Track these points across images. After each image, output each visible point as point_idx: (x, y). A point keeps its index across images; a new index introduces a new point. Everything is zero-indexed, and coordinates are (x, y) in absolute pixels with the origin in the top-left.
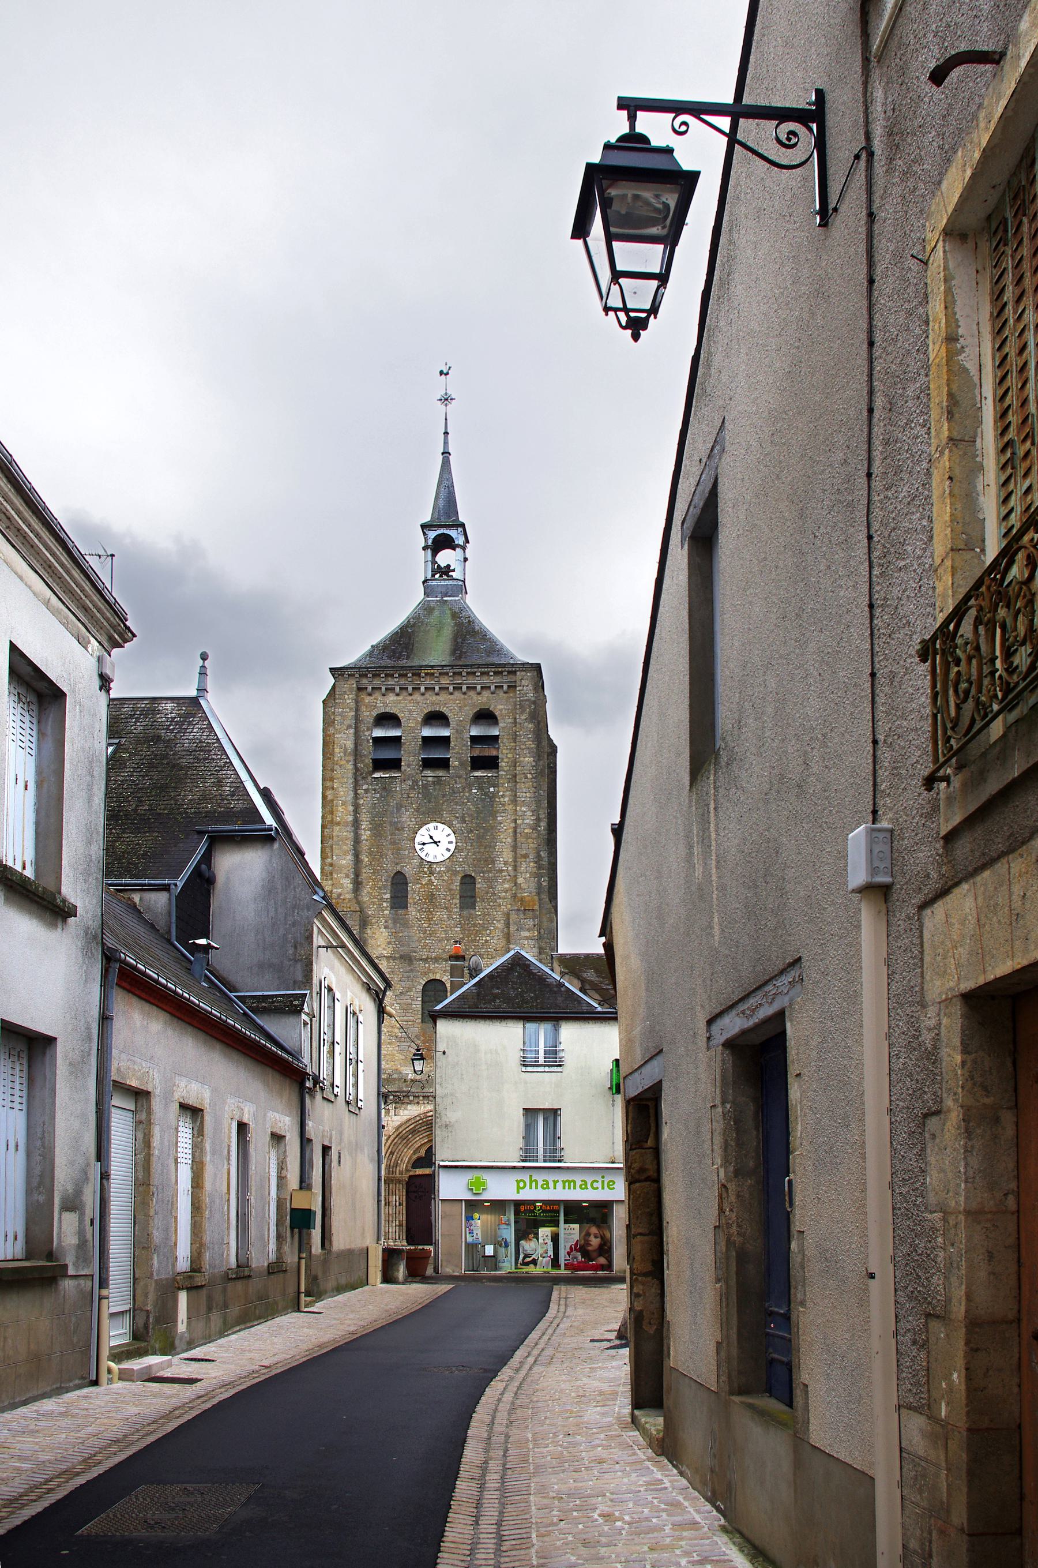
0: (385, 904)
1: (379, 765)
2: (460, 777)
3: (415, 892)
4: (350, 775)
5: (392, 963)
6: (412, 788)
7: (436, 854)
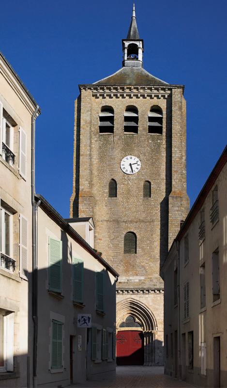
0: (105, 195)
1: (102, 129)
2: (143, 135)
3: (120, 188)
4: (88, 133)
5: (109, 224)
6: (119, 139)
7: (134, 159)
